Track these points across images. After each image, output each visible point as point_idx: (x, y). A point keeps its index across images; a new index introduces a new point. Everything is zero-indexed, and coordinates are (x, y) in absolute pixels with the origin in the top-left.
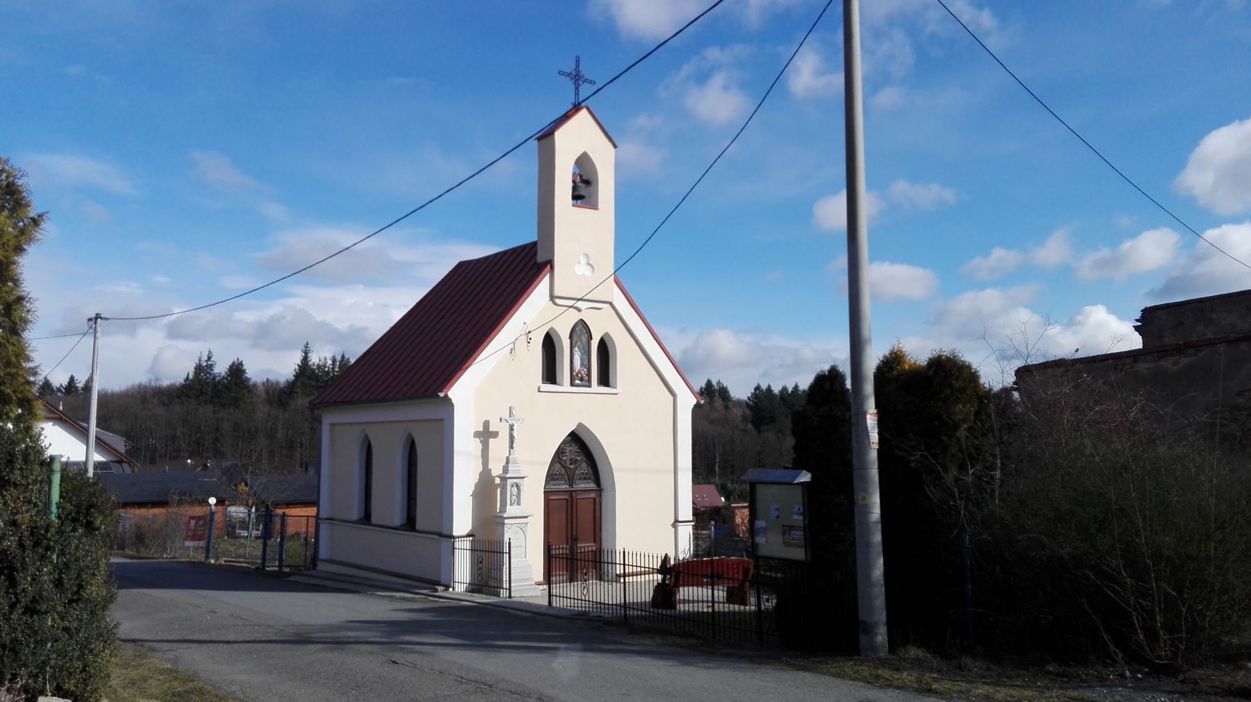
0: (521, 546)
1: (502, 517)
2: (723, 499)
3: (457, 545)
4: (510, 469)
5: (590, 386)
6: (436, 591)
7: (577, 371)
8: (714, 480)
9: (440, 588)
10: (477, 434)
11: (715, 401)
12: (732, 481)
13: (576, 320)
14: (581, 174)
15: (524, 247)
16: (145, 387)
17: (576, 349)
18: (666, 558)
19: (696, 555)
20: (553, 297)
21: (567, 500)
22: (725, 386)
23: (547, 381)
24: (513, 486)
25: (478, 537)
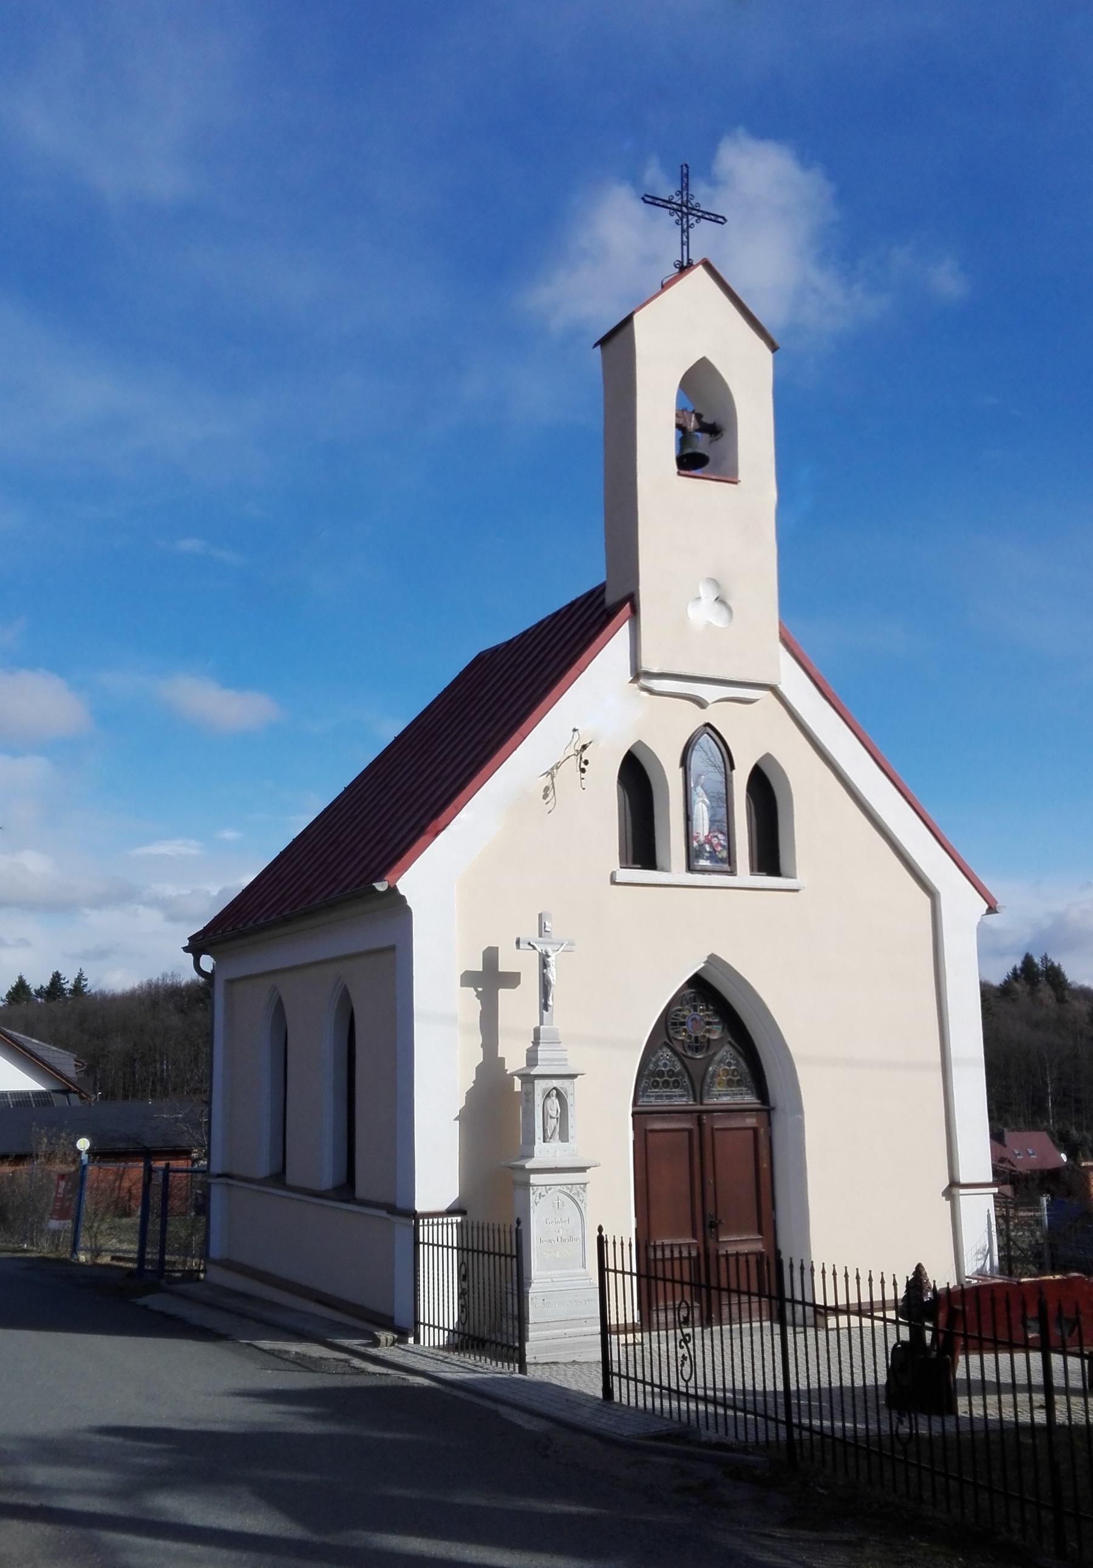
0: (571, 1239)
1: (522, 1168)
2: (1064, 1157)
3: (424, 1233)
4: (540, 1055)
5: (732, 872)
6: (376, 1343)
7: (702, 839)
8: (1045, 1124)
9: (385, 1336)
10: (469, 979)
11: (1039, 991)
12: (1079, 1127)
13: (697, 727)
14: (698, 411)
15: (591, 593)
16: (157, 986)
17: (699, 789)
18: (919, 1276)
19: (1008, 1261)
20: (637, 674)
21: (690, 1131)
22: (1056, 964)
23: (635, 862)
24: (548, 1096)
25: (477, 1216)
